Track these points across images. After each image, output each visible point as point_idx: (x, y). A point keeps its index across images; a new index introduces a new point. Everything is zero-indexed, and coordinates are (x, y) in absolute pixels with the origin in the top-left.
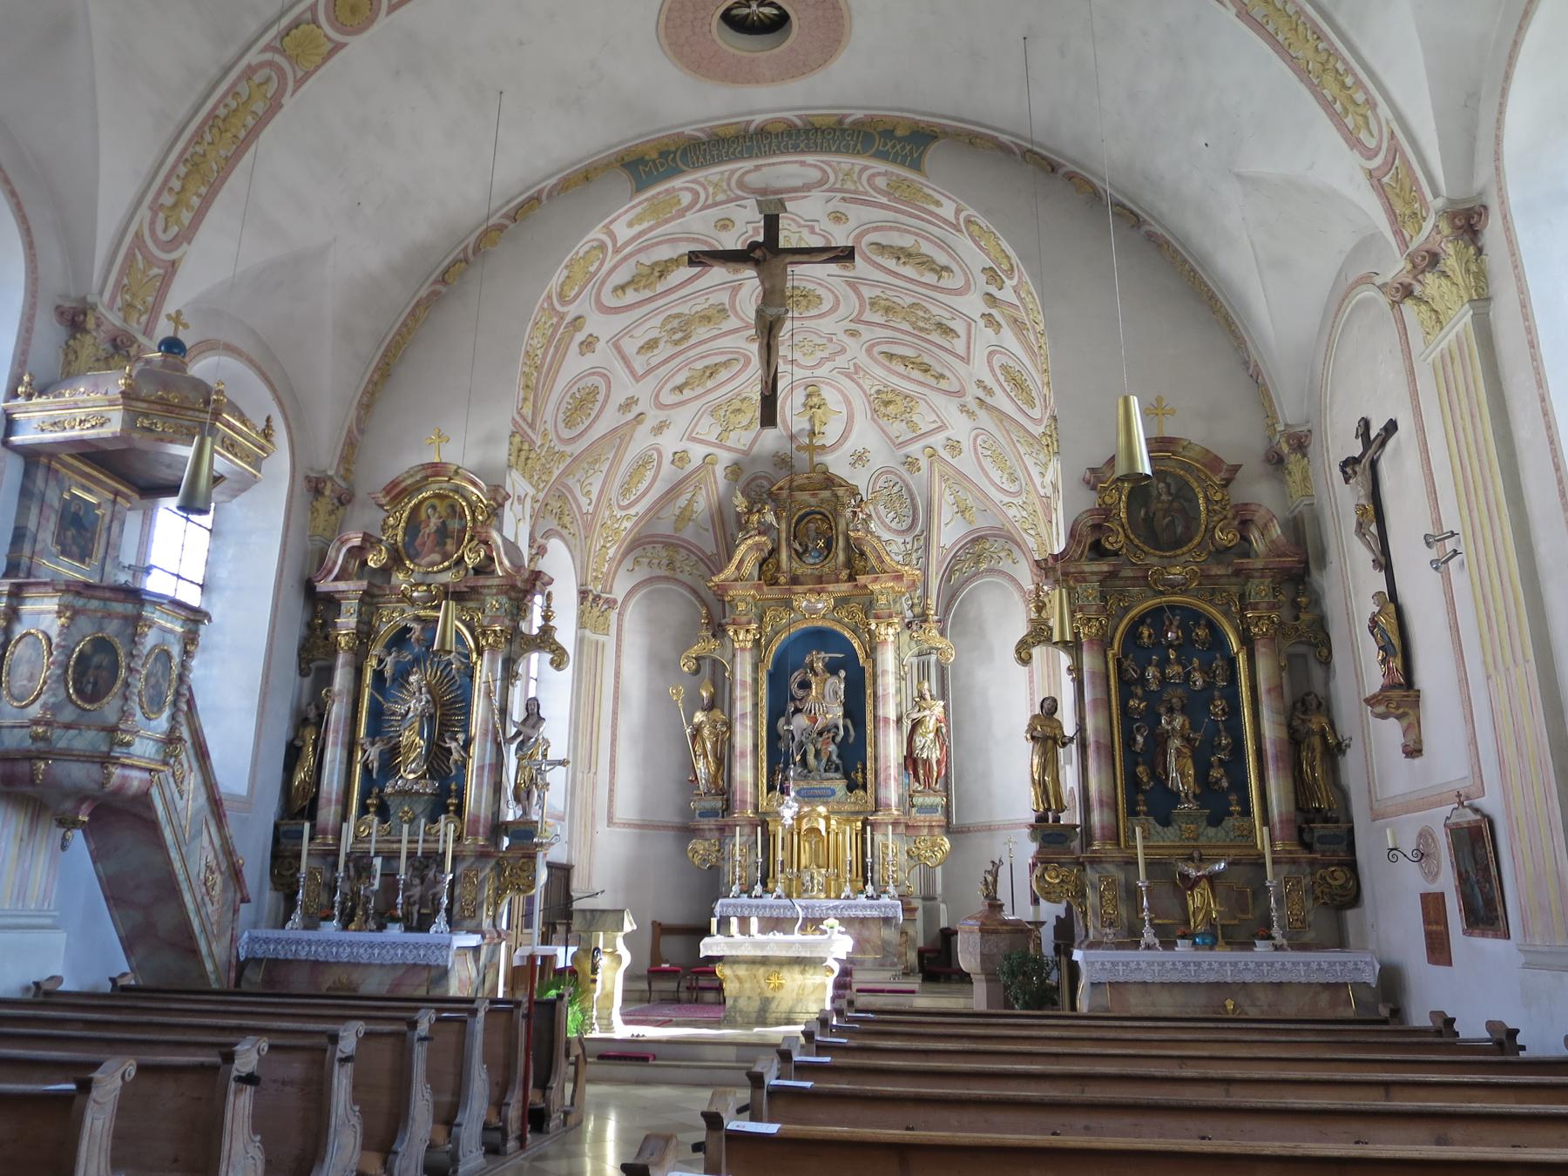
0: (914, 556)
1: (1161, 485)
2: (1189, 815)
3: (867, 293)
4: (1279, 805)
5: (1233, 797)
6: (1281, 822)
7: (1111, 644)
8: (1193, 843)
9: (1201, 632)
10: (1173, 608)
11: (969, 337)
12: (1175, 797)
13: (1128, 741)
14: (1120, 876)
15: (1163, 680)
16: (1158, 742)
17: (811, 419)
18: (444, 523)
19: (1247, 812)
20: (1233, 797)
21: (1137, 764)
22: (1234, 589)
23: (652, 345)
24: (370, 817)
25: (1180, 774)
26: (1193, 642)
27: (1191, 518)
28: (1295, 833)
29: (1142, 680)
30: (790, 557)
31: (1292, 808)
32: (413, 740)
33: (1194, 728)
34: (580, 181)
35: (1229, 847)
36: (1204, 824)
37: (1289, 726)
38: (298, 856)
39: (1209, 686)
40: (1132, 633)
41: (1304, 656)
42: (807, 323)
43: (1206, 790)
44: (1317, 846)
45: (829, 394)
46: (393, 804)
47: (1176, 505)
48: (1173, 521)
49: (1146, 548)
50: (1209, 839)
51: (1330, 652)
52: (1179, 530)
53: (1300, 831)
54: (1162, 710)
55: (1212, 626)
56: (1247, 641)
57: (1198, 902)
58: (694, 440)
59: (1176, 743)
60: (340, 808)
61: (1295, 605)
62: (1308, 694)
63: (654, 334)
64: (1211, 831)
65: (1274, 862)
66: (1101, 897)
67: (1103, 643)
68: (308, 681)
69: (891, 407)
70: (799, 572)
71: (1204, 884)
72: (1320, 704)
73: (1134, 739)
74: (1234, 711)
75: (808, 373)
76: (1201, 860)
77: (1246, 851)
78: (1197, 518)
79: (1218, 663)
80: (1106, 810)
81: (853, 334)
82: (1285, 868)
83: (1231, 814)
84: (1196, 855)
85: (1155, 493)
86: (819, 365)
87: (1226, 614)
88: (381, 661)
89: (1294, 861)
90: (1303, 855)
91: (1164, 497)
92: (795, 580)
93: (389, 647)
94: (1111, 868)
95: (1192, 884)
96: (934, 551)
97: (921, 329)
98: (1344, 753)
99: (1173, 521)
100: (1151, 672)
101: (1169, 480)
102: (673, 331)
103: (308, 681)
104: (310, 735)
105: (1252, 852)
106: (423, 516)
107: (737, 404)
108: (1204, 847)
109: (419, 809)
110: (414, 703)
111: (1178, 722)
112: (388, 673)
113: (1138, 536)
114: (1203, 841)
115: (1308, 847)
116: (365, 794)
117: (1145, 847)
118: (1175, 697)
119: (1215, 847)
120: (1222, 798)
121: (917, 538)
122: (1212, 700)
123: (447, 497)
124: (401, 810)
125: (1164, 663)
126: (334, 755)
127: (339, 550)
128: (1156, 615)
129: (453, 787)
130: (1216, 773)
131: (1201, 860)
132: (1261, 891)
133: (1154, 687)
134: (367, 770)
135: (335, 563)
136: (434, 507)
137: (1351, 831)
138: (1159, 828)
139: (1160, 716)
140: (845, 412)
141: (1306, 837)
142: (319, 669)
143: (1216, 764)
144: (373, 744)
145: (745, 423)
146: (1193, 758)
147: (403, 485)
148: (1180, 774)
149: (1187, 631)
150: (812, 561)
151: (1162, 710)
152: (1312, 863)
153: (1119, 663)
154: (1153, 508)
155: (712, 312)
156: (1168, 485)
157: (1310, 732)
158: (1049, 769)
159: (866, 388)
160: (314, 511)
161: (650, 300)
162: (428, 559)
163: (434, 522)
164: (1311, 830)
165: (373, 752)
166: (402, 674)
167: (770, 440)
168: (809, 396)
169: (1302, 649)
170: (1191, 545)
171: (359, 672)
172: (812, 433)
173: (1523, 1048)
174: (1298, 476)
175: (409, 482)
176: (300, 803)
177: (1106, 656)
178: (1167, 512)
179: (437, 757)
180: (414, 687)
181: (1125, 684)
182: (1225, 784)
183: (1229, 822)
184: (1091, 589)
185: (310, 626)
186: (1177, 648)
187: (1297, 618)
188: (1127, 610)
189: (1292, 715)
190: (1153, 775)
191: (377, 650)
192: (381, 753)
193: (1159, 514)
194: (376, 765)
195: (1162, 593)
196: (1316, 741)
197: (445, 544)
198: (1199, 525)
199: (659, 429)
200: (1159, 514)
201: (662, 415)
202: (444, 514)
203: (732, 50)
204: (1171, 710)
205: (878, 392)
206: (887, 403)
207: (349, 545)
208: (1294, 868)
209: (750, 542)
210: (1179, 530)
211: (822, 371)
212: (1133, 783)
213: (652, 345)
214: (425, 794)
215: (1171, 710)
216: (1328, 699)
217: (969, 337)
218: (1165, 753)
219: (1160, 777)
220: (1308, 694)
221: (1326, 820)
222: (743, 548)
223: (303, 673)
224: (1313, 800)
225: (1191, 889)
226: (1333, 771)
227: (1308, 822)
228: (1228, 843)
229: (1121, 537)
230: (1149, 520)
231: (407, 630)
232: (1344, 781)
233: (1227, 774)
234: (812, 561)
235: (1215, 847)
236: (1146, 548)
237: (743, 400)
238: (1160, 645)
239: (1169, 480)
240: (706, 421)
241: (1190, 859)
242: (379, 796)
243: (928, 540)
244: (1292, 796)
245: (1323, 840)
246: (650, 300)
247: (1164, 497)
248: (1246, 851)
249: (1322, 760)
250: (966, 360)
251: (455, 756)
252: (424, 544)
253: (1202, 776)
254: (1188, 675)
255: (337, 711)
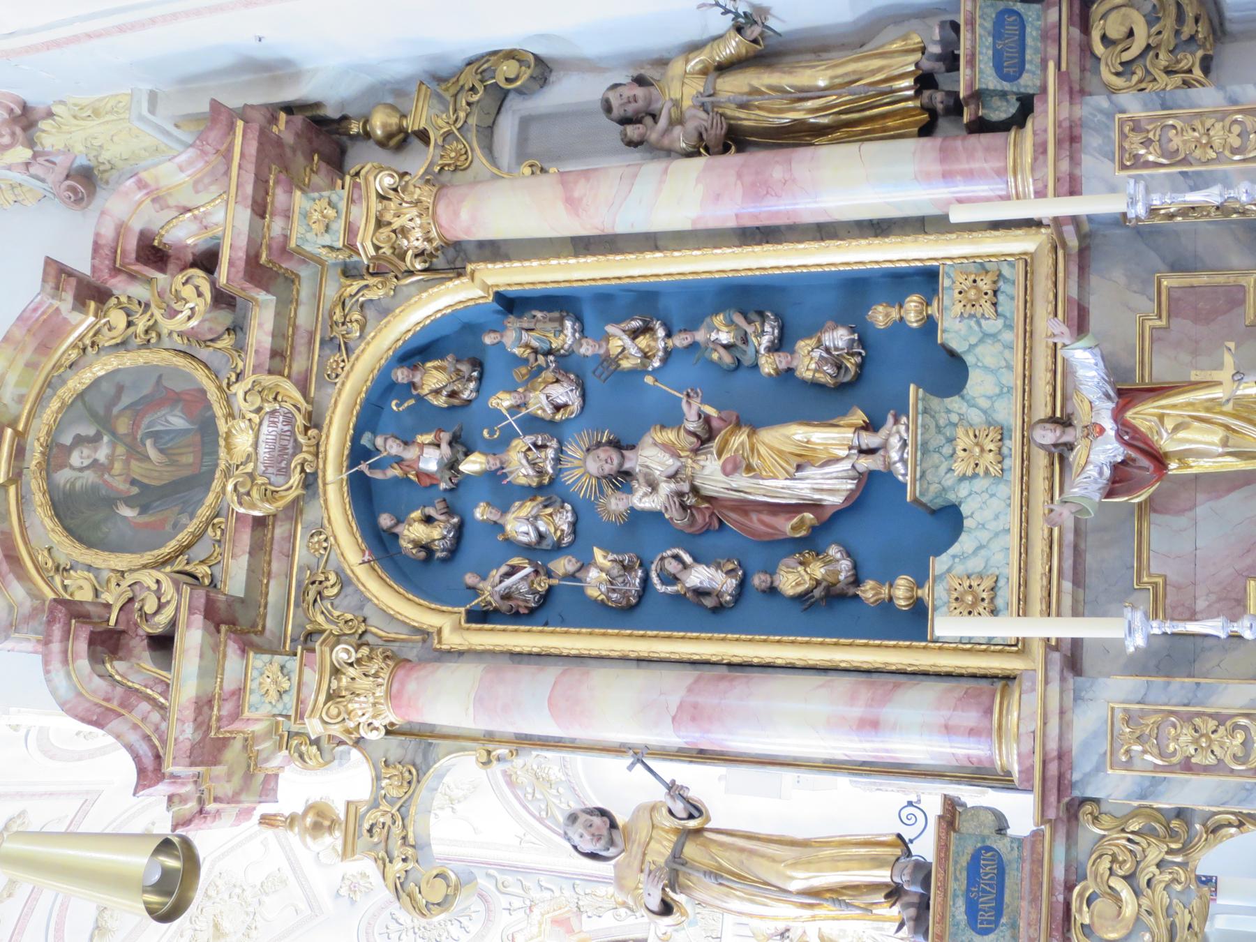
0: (535, 894)
1: (76, 459)
2: (925, 449)
4: (965, 90)
5: (881, 316)
6: (947, 176)
8: (1014, 444)
9: (433, 378)
10: (358, 453)
11: (21, 795)
12: (873, 487)
13: (707, 612)
14: (1113, 692)
15: (547, 490)
16: (708, 521)
19: (926, 279)
20: (881, 316)
21: (772, 591)
25: (810, 463)
26: (458, 406)
28: (986, 139)
29: (540, 551)
31: (911, 145)
33: (672, 419)
35: (1029, 334)
36: (954, 403)
39: (566, 364)
40: (417, 571)
41: (526, 123)
43: (851, 391)
44: (1027, 83)
48: (156, 436)
49: (204, 512)
50: (1004, 391)
51: (511, 55)
52: (177, 421)
53: (981, 126)
54: (616, 504)
55: (417, 353)
56: (451, 259)
57: (1209, 438)
59: (712, 474)
61: (399, 140)
64: (978, 384)
65: (1073, 187)
66: (1187, 766)
67: (409, 655)
69: (226, 925)
71: (1143, 416)
72: (640, 81)
73: (700, 593)
74: (644, 306)
76: (1065, 422)
77: (1043, 286)
78: (160, 375)
79: (513, 338)
80: (890, 712)
82: (1092, 164)
83: (930, 326)
84: (1047, 436)
85: (90, 477)
89: (1071, 138)
90: (1048, 115)
91: (102, 454)
94: (1087, 722)
95: (1143, 462)
96: (527, 858)
99: (156, 436)
101: (67, 440)
105: (1044, 268)
108: (1027, 409)
111: (652, 457)
113: (177, 527)
114: (1008, 412)
115: (1026, 106)
117: (1023, 608)
118: (586, 466)
119: (1028, 379)
120: (882, 348)
121: (502, 888)
122: (608, 363)
125: (498, 487)
128: (364, 494)
130: (808, 361)
131: (1065, 422)
132: (1152, 239)
133: (563, 520)
138: (965, 543)
141: (1002, 111)
143: (782, 361)
148: (810, 463)
149: (425, 417)
151: (616, 504)
152: (1075, 91)
153: (480, 616)
154: (121, 485)
156: (79, 441)
157: (708, 104)
158: (762, 870)
164: (978, 96)
169: (507, 128)
170: (213, 394)
174: (96, 129)
178: (135, 452)
181: (538, 610)
182: (839, 338)
183: (954, 331)
184: (263, 681)
186: (462, 444)
187: (423, 136)
190: (808, 546)
193: (137, 469)
195: (310, 482)
196: (733, 85)
198: (176, 369)
200: (137, 469)
204: (622, 479)
208: (1091, 140)
212: (828, 608)
215: (622, 479)
216: (632, 60)
218: (745, 507)
219: (823, 527)
220: (608, 108)
221: (951, 61)
225: (1159, 460)
226: (815, 46)
228: (1013, 337)
229: (148, 578)
230: (146, 497)
233: (813, 330)
235: (1028, 379)
236: (204, 512)
238: (453, 495)
239: (67, 440)
241: (1061, 454)
243: (504, 868)
245: (1010, 62)
247: (102, 454)
248: (1043, 286)
254: (533, 424)
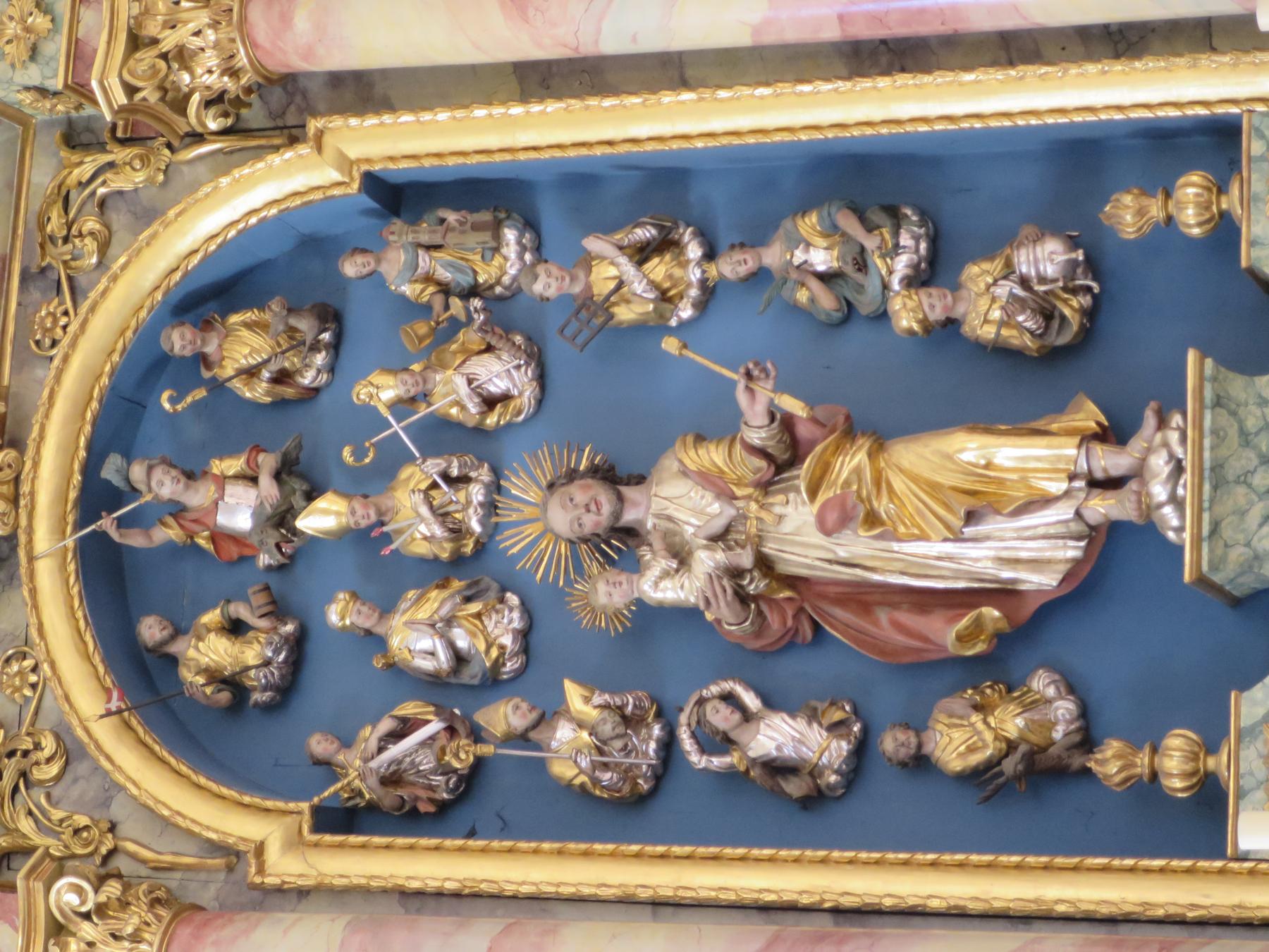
7: (231, 855)
10: (96, 497)
12: (1117, 555)
15: (470, 567)
16: (790, 624)
21: (920, 763)
26: (292, 400)
33: (718, 424)
39: (504, 316)
54: (608, 593)
55: (210, 296)
59: (798, 532)
73: (777, 768)
74: (659, 197)
79: (400, 265)
83: (1225, 232)
87: (147, 214)
100: (416, 640)
111: (679, 499)
122: (591, 311)
125: (375, 561)
133: (504, 627)
139: (647, 617)
143: (934, 304)
146: (877, 428)
151: (608, 593)
153: (341, 819)
173: (1099, 424)
177: (298, 896)
182: (1046, 258)
186: (301, 477)
188: (71, 752)
190: (991, 671)
203: (1081, 282)
204: (620, 543)
215: (620, 543)
218: (864, 596)
219: (1020, 634)
233: (996, 243)
253: (1014, 383)
254: (441, 435)
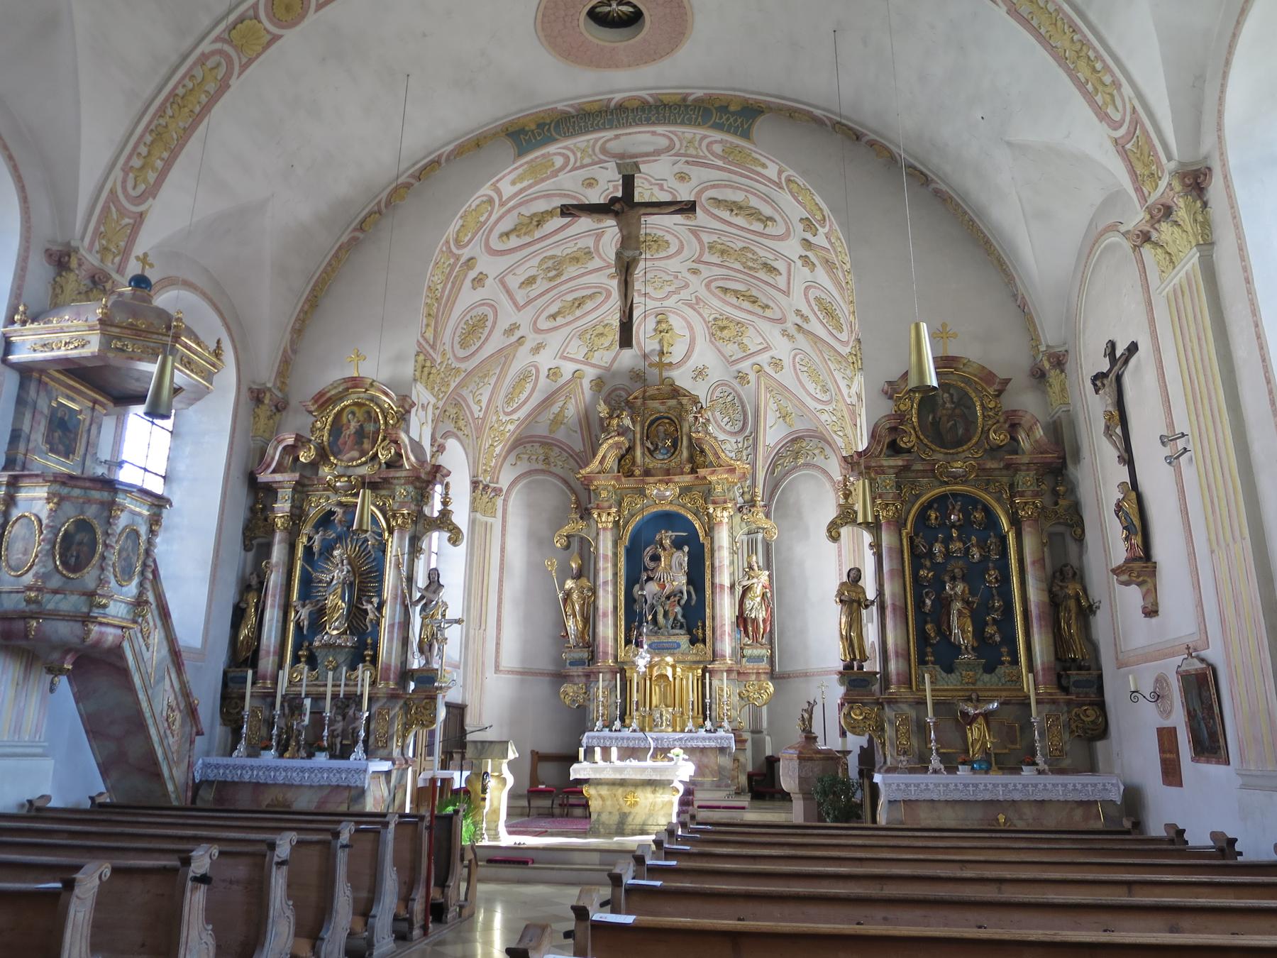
0: (745, 453)
1: (946, 395)
2: (968, 664)
3: (706, 238)
4: (1042, 656)
5: (1004, 650)
6: (1043, 669)
8: (971, 687)
9: (978, 515)
10: (955, 495)
11: (789, 275)
12: (957, 649)
13: (919, 604)
14: (912, 714)
15: (948, 554)
16: (943, 604)
17: (661, 341)
18: (361, 426)
19: (1015, 661)
20: (1004, 650)
21: (926, 623)
22: (1005, 480)
23: (531, 281)
24: (301, 665)
25: (961, 630)
26: (972, 523)
27: (970, 422)
28: (1054, 678)
29: (930, 554)
30: (643, 454)
31: (1053, 659)
32: (337, 603)
33: (972, 593)
34: (473, 148)
35: (1001, 690)
36: (981, 671)
37: (1050, 591)
38: (243, 697)
39: (985, 559)
40: (922, 516)
41: (1062, 535)
42: (657, 263)
43: (982, 643)
44: (1073, 689)
45: (675, 321)
46: (320, 655)
47: (957, 411)
48: (955, 425)
49: (933, 447)
50: (985, 684)
51: (1083, 531)
52: (960, 431)
53: (1059, 677)
54: (947, 578)
55: (987, 510)
56: (1016, 522)
57: (976, 735)
58: (565, 358)
59: (958, 605)
60: (277, 658)
61: (1055, 493)
62: (1066, 565)
63: (533, 272)
64: (986, 677)
65: (1038, 702)
66: (897, 731)
67: (899, 524)
68: (251, 555)
69: (726, 331)
70: (651, 466)
71: (981, 720)
72: (1075, 574)
73: (924, 602)
74: (1005, 579)
75: (658, 304)
76: (978, 700)
77: (1014, 694)
78: (975, 422)
79: (992, 540)
80: (901, 660)
81: (695, 272)
82: (1047, 707)
83: (1002, 663)
84: (974, 696)
85: (940, 402)
86: (667, 297)
88: (310, 539)
89: (1054, 702)
90: (1062, 697)
91: (948, 405)
92: (647, 473)
93: (316, 527)
94: (905, 707)
95: (971, 720)
96: (761, 449)
97: (750, 268)
98: (1094, 613)
99: (955, 425)
101: (952, 391)
102: (548, 269)
103: (251, 555)
104: (252, 599)
105: (1019, 694)
106: (345, 420)
107: (600, 329)
108: (980, 690)
109: (341, 659)
110: (337, 573)
111: (960, 588)
112: (316, 548)
113: (927, 437)
114: (979, 685)
115: (1065, 690)
116: (297, 647)
117: (933, 690)
118: (957, 567)
119: (989, 690)
120: (996, 650)
121: (747, 438)
122: (987, 570)
123: (364, 405)
124: (326, 659)
125: (948, 540)
126: (272, 615)
127: (276, 448)
128: (941, 501)
129: (369, 641)
130: (990, 630)
131: (978, 700)
132: (1027, 726)
133: (940, 560)
134: (299, 627)
135: (273, 459)
136: (353, 413)
137: (1100, 677)
138: (944, 675)
140: (688, 336)
141: (1064, 682)
142: (260, 545)
143: (990, 622)
144: (304, 606)
145: (606, 345)
147: (328, 395)
148: (961, 630)
149: (966, 514)
150: (661, 457)
151: (947, 578)
152: (1069, 703)
153: (911, 540)
154: (939, 414)
155: (580, 254)
156: (951, 395)
157: (1067, 597)
158: (854, 626)
159: (706, 316)
160: (256, 416)
161: (529, 244)
162: (349, 455)
163: (354, 425)
164: (1068, 676)
165: (304, 613)
166: (328, 549)
167: (627, 358)
168: (659, 322)
169: (1060, 529)
170: (970, 444)
171: (292, 548)
172: (662, 353)
174: (1057, 388)
175: (333, 392)
176: (244, 654)
178: (950, 417)
179: (356, 617)
180: (337, 560)
181: (916, 557)
182: (998, 638)
183: (1001, 670)
184: (889, 480)
185: (252, 510)
186: (959, 528)
187: (1056, 503)
189: (1052, 582)
190: (939, 631)
191: (307, 529)
192: (310, 613)
193: (944, 419)
194: (306, 623)
195: (947, 483)
196: (1072, 604)
197: (362, 443)
198: (977, 428)
199: (537, 349)
200: (944, 419)
201: (539, 338)
202: (361, 419)
204: (953, 579)
205: (715, 319)
206: (723, 329)
207: (284, 444)
208: (1054, 707)
209: (610, 441)
210: (960, 431)
211: (669, 302)
212: (922, 638)
213: (531, 281)
214: (346, 647)
215: (953, 579)
216: (1081, 569)
217: (789, 275)
218: (949, 614)
219: (944, 633)
220: (1066, 565)
221: (1080, 668)
222: (605, 446)
223: (247, 548)
224: (1069, 651)
225: (970, 724)
226: (1086, 628)
227: (1065, 669)
228: (1000, 686)
229: (913, 438)
230: (936, 424)
231: (332, 513)
232: (1094, 636)
233: (1000, 630)
234: (661, 457)
235: (989, 690)
236: (933, 447)
237: (605, 326)
238: (944, 526)
239: (952, 391)
240: (575, 343)
241: (969, 699)
242: (308, 649)
243: (756, 440)
244: (1052, 648)
245: (1077, 684)
246: (529, 244)
247: (948, 405)
248: (1014, 694)
249: (1077, 619)
250: (787, 293)
251: (371, 616)
252: (345, 443)
254: (967, 550)
255: (275, 579)
